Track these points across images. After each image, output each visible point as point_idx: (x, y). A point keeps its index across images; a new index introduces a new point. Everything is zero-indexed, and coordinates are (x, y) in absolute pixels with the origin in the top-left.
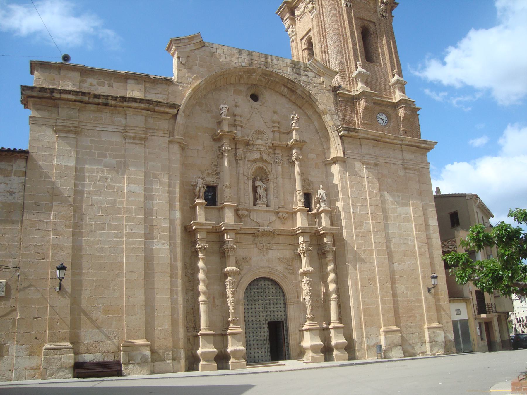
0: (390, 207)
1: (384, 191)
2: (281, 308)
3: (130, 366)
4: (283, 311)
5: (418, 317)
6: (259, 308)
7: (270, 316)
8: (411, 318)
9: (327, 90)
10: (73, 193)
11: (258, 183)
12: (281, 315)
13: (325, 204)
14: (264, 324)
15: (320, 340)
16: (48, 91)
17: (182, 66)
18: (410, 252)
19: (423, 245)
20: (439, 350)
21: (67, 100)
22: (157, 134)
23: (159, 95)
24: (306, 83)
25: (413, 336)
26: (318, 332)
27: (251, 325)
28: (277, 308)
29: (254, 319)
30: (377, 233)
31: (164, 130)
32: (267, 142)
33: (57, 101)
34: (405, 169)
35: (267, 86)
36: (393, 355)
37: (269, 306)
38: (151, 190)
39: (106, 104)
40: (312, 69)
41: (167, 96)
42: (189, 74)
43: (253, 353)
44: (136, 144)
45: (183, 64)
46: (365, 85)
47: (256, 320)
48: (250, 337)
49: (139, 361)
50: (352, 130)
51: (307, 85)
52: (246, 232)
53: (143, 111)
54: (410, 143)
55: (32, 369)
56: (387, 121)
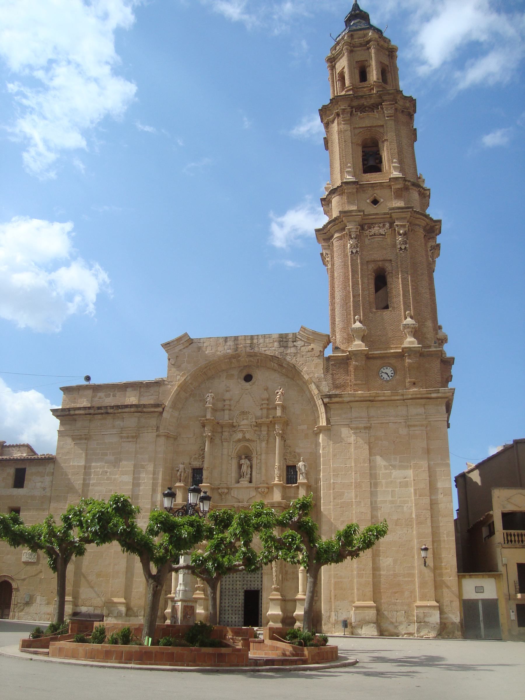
0: (381, 473)
2: (258, 578)
3: (109, 618)
5: (407, 594)
6: (236, 578)
7: (247, 585)
8: (396, 594)
9: (316, 357)
10: (81, 486)
11: (243, 461)
12: (258, 585)
14: (240, 592)
16: (67, 410)
18: (404, 520)
19: (424, 511)
20: (429, 632)
21: (80, 414)
22: (146, 431)
23: (151, 397)
24: (293, 355)
25: (398, 614)
26: (279, 602)
28: (254, 578)
29: (231, 587)
31: (152, 427)
33: (75, 417)
34: (409, 426)
35: (259, 364)
37: (247, 576)
38: (139, 478)
39: (107, 413)
40: (300, 338)
42: (178, 372)
43: (227, 618)
45: (173, 365)
47: (233, 588)
48: (225, 603)
49: (116, 614)
50: (333, 396)
51: (294, 356)
54: (414, 396)
56: (392, 375)
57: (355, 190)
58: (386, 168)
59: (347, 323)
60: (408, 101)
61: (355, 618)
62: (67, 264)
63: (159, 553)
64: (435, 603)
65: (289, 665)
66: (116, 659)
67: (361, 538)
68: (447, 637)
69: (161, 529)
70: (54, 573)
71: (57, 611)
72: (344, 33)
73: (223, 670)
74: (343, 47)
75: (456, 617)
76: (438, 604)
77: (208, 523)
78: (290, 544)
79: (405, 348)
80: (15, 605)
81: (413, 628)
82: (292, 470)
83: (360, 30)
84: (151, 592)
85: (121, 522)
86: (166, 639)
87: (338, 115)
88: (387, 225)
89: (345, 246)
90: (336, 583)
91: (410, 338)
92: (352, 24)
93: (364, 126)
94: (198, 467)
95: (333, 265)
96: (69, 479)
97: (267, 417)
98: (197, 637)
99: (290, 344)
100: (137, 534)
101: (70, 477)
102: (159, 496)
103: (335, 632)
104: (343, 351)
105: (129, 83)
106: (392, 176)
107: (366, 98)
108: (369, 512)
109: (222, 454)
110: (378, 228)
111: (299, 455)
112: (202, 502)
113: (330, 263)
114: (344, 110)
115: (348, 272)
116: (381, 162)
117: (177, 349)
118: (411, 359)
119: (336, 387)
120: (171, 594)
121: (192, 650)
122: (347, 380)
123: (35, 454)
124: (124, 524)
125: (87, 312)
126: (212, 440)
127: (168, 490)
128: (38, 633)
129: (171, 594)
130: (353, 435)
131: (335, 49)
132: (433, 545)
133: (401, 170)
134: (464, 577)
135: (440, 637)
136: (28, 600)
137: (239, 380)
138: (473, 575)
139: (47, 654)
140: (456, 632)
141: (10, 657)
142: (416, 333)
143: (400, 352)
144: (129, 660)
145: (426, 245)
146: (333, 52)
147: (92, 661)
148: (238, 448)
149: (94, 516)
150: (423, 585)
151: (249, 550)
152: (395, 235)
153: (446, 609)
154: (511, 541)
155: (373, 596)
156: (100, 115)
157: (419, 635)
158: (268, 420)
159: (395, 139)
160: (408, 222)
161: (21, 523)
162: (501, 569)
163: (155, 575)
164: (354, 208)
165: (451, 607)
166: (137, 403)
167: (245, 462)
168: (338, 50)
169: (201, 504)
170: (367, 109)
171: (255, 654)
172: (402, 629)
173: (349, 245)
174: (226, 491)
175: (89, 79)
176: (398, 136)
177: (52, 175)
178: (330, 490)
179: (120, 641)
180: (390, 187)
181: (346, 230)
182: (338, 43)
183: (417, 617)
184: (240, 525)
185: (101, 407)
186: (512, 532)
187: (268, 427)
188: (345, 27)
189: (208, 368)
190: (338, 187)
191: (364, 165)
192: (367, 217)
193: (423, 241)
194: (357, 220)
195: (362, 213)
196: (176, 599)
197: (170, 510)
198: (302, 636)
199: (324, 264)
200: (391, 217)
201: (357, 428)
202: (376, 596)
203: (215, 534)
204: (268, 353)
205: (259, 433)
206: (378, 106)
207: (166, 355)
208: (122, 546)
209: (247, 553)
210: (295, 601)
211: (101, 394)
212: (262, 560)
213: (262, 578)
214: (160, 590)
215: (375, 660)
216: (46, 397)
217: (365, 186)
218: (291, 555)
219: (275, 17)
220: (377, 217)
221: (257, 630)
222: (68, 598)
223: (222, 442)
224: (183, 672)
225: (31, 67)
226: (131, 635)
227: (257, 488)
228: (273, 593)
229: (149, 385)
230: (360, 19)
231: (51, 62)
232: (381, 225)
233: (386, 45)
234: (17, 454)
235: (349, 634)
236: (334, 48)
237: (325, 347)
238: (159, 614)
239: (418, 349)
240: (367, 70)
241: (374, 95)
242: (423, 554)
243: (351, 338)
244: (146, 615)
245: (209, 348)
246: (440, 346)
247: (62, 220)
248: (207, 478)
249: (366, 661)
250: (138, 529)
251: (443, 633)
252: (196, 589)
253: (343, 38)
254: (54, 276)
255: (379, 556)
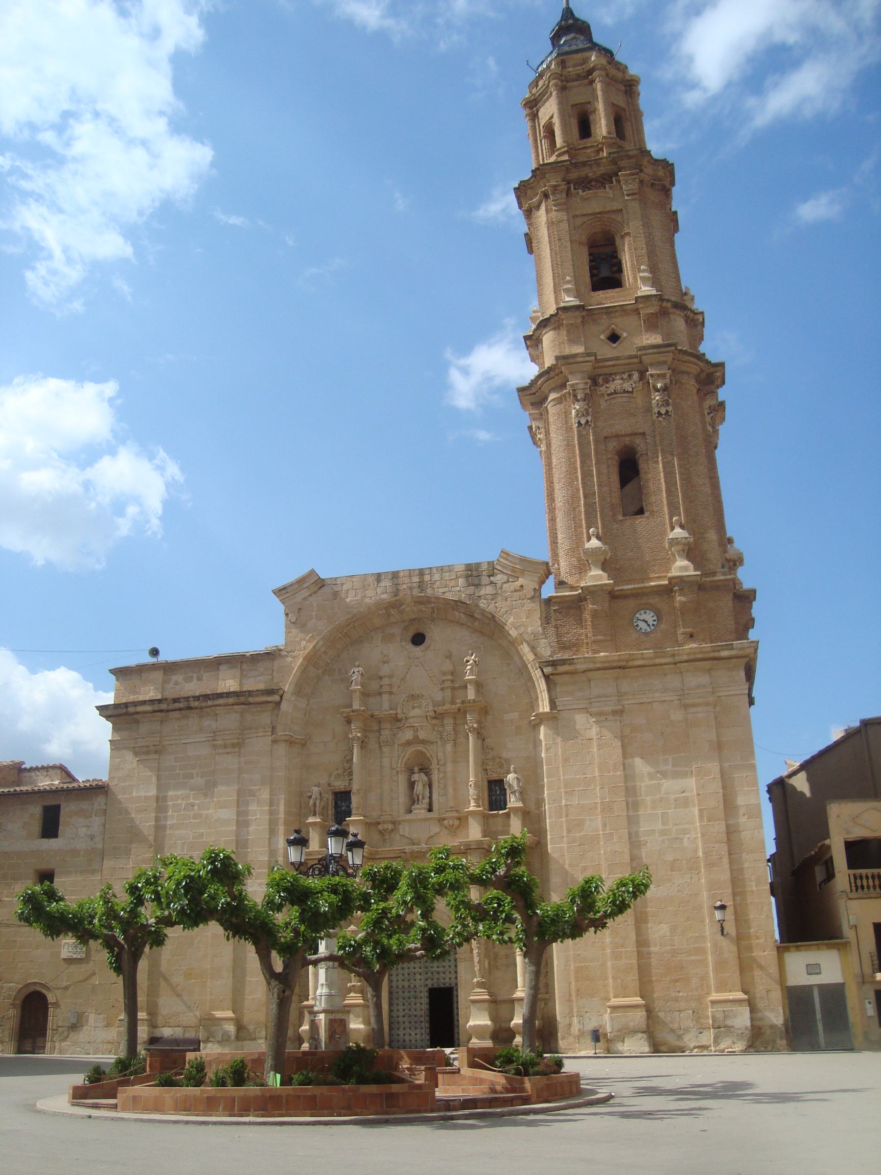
0: (644, 784)
1: (633, 757)
3: (210, 1045)
4: (453, 972)
5: (694, 981)
8: (678, 984)
11: (415, 777)
12: (450, 978)
13: (515, 796)
14: (421, 992)
15: (488, 1019)
16: (123, 706)
17: (292, 625)
18: (684, 862)
19: (716, 845)
20: (734, 1043)
21: (146, 712)
22: (255, 735)
23: (261, 678)
25: (681, 1015)
26: (486, 1005)
27: (401, 993)
28: (444, 967)
29: (406, 984)
30: (611, 835)
32: (427, 710)
33: (136, 716)
34: (686, 707)
35: (435, 615)
36: (626, 1048)
39: (190, 708)
41: (270, 677)
42: (302, 635)
44: (228, 753)
45: (293, 623)
46: (603, 571)
49: (219, 1038)
50: (560, 662)
51: (492, 600)
52: (388, 856)
53: (236, 707)
54: (692, 657)
55: (109, 1042)
56: (655, 623)
57: (580, 320)
58: (628, 279)
59: (577, 542)
60: (660, 167)
61: (612, 1026)
62: (112, 452)
63: (286, 936)
64: (741, 995)
65: (501, 1107)
66: (224, 1110)
67: (609, 898)
68: (763, 1049)
69: (285, 900)
70: (118, 976)
71: (126, 1038)
72: (549, 59)
73: (395, 1118)
74: (549, 82)
75: (776, 1017)
76: (746, 997)
77: (359, 884)
78: (495, 912)
79: (674, 578)
80: (53, 1030)
81: (708, 1037)
82: (497, 788)
83: (577, 51)
84: (276, 1000)
85: (222, 891)
86: (303, 1075)
87: (546, 196)
88: (636, 376)
89: (567, 414)
90: (578, 970)
91: (682, 561)
92: (562, 42)
93: (590, 212)
94: (343, 790)
95: (549, 446)
96: (132, 820)
97: (453, 702)
98: (352, 1068)
99: (485, 580)
100: (248, 909)
101: (133, 816)
102: (281, 842)
103: (579, 1051)
104: (572, 588)
105: (199, 146)
106: (639, 294)
107: (591, 165)
108: (627, 851)
109: (381, 767)
110: (621, 382)
111: (508, 762)
112: (351, 850)
113: (544, 442)
114: (555, 186)
115: (575, 457)
116: (620, 270)
117: (299, 597)
118: (684, 596)
119: (563, 647)
120: (308, 1000)
121: (344, 1090)
122: (580, 635)
123: (74, 780)
124: (226, 894)
125: (149, 533)
126: (364, 744)
127: (295, 835)
128: (97, 1074)
129: (308, 1000)
130: (594, 725)
131: (537, 86)
132: (734, 900)
133: (655, 282)
134: (787, 949)
135: (752, 1050)
136: (74, 1021)
137: (404, 643)
138: (800, 946)
139: (115, 1107)
140: (778, 1041)
141: (55, 1114)
142: (692, 552)
143: (665, 585)
144: (245, 1110)
145: (701, 405)
146: (534, 91)
147: (187, 1115)
148: (407, 755)
149: (178, 883)
150: (720, 965)
151: (432, 924)
152: (649, 390)
153: (760, 1005)
154: (862, 887)
155: (640, 988)
156: (153, 201)
157: (717, 1048)
158: (453, 706)
159: (642, 231)
160: (669, 369)
161: (61, 899)
162: (848, 933)
163: (280, 973)
164: (580, 349)
165: (768, 1000)
166: (238, 690)
167: (419, 778)
168: (542, 87)
169: (349, 854)
170: (593, 183)
171: (446, 1091)
172: (690, 1040)
173: (573, 411)
174: (390, 826)
175: (131, 142)
176: (647, 225)
177: (78, 306)
178: (561, 817)
179: (229, 1081)
180: (637, 311)
181: (568, 387)
182: (541, 76)
183: (712, 1019)
184: (412, 888)
185: (178, 699)
186: (863, 872)
187: (455, 718)
188: (551, 49)
189: (351, 626)
190: (552, 316)
191: (592, 276)
192: (601, 364)
193: (696, 398)
194: (585, 369)
195: (593, 358)
196: (316, 1009)
197: (299, 866)
198: (521, 1060)
199: (535, 443)
200: (641, 362)
201: (600, 714)
202: (645, 988)
203: (374, 904)
204: (449, 596)
205: (441, 729)
206: (612, 178)
207: (282, 607)
208: (226, 929)
209: (427, 929)
210: (513, 1001)
211: (178, 677)
212: (452, 939)
213: (456, 966)
214: (290, 997)
215: (642, 1093)
216: (86, 678)
217: (595, 312)
218: (498, 929)
219: (440, 21)
220: (618, 362)
221: (452, 1053)
222: (142, 1015)
223: (380, 747)
224: (332, 1126)
225: (33, 127)
226: (247, 1071)
227: (441, 820)
228: (475, 991)
229: (255, 659)
230: (577, 33)
231: (67, 115)
232: (625, 376)
233: (620, 75)
234: (44, 783)
235: (603, 1053)
236: (535, 83)
237: (543, 582)
238: (290, 1033)
239: (694, 579)
240: (591, 118)
241: (605, 160)
242: (718, 915)
243: (584, 565)
244: (268, 1038)
245: (351, 594)
246: (732, 572)
247: (99, 379)
248: (358, 808)
249: (625, 1094)
250: (249, 901)
251: (757, 1044)
252: (350, 990)
253: (548, 67)
254: (89, 473)
255: (646, 922)
